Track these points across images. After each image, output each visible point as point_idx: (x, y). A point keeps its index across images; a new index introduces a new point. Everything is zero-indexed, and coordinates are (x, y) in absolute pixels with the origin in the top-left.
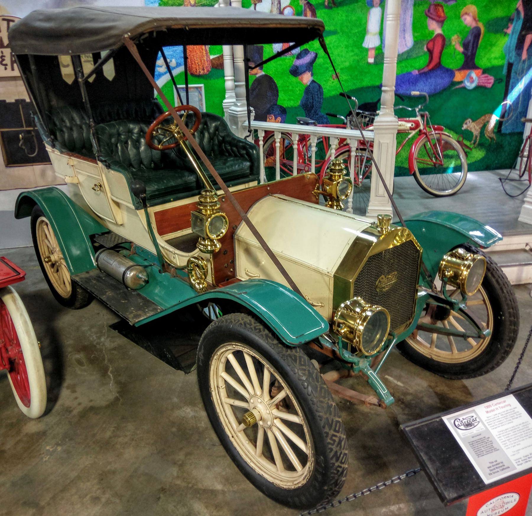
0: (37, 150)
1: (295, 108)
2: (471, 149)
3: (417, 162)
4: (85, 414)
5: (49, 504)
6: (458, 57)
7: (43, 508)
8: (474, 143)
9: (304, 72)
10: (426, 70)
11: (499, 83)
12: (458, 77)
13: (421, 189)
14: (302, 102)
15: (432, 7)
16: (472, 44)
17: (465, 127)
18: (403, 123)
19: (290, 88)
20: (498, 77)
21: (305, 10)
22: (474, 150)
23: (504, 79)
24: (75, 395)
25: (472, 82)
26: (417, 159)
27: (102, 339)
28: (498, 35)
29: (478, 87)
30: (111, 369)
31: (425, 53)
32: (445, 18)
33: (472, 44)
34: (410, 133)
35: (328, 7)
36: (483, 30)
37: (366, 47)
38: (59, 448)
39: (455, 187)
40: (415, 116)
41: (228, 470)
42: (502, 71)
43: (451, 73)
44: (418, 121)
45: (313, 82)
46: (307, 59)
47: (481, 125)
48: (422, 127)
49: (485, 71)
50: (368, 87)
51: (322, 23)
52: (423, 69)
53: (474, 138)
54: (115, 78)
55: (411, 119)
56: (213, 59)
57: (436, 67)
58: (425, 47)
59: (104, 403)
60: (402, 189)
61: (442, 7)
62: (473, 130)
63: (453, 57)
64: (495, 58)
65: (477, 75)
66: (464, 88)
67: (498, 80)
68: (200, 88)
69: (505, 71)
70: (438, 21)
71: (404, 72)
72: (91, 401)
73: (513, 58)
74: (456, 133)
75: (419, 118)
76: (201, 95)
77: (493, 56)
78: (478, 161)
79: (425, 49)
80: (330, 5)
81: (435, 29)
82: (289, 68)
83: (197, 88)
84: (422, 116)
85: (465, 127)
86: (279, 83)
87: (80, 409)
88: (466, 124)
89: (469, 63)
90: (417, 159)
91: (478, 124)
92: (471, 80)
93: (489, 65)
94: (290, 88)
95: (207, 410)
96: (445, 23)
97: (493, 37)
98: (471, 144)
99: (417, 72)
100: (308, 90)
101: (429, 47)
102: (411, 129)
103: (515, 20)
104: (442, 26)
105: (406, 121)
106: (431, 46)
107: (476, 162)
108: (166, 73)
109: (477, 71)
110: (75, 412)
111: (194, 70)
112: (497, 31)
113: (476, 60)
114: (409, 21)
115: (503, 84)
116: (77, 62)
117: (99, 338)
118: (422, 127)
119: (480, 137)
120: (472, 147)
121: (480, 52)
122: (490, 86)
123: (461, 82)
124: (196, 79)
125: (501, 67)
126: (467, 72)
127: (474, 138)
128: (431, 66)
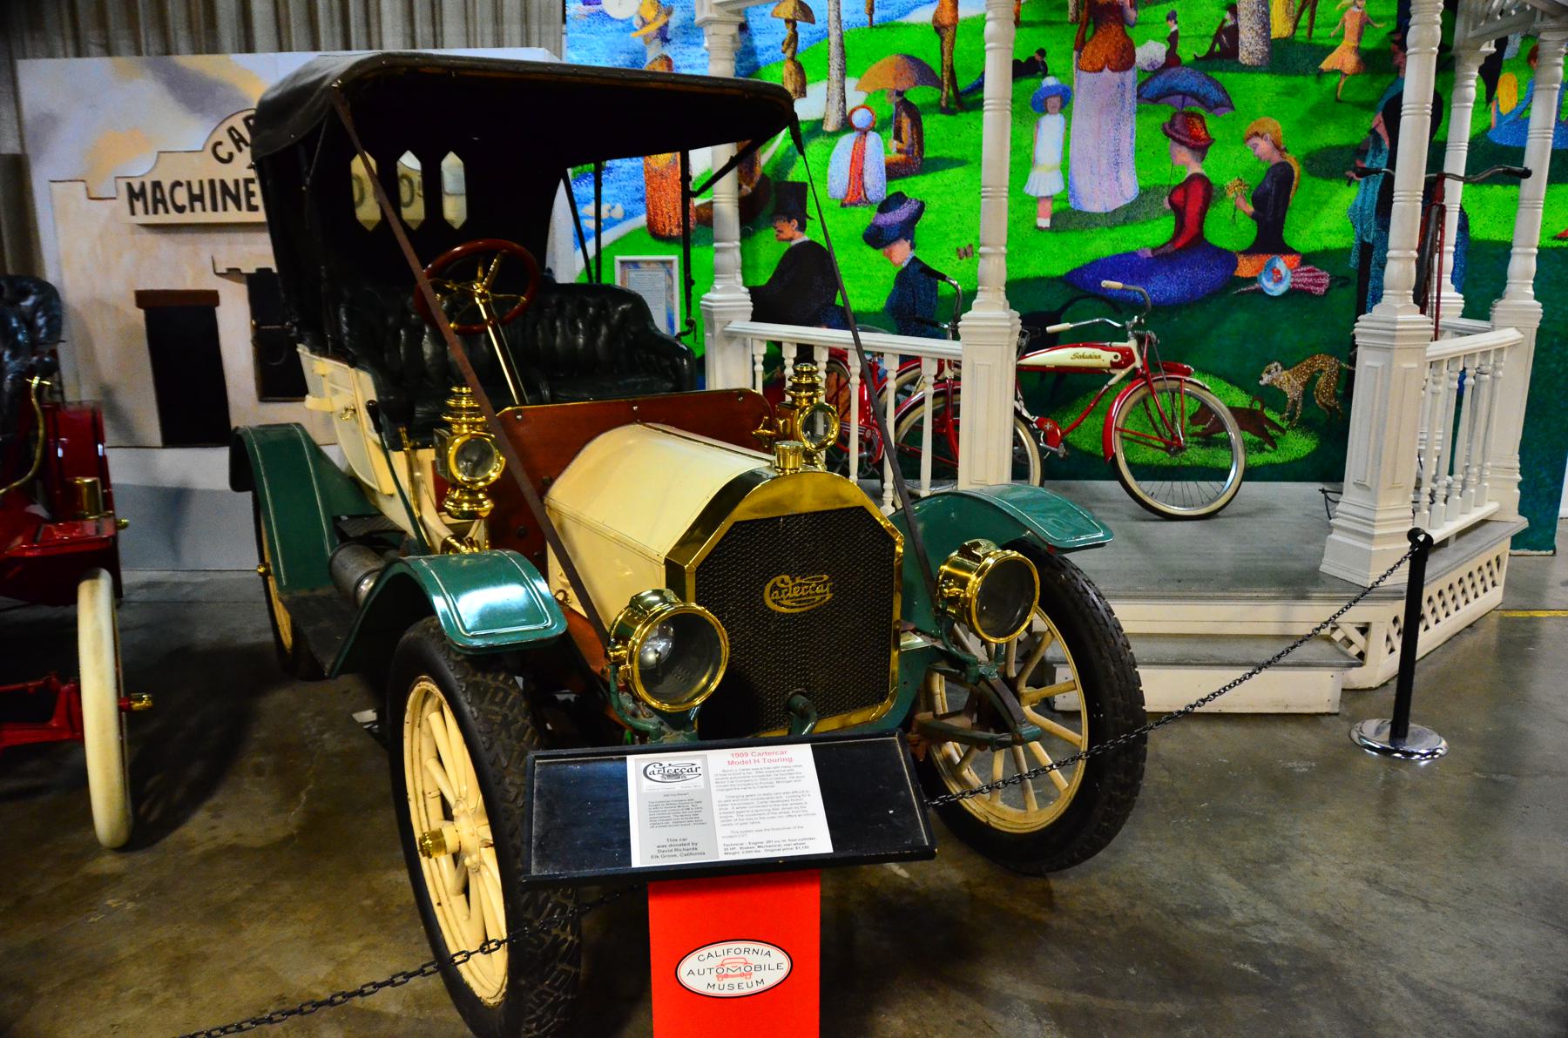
0: (723, 634)
1: (875, 313)
2: (1283, 431)
3: (1122, 437)
4: (209, 858)
5: (53, 993)
6: (1242, 225)
7: (40, 996)
8: (1291, 418)
9: (896, 239)
10: (1170, 249)
11: (1342, 286)
12: (1245, 268)
13: (1128, 497)
14: (890, 300)
15: (1179, 118)
16: (1272, 202)
17: (1266, 379)
18: (1097, 352)
19: (864, 270)
20: (1339, 273)
21: (897, 115)
22: (1289, 433)
23: (1354, 277)
24: (213, 822)
25: (1280, 280)
26: (1121, 430)
27: (326, 736)
28: (1333, 184)
29: (1292, 293)
30: (310, 786)
31: (1165, 214)
32: (1209, 141)
33: (1272, 202)
34: (1113, 376)
35: (946, 111)
36: (1297, 169)
37: (1033, 194)
38: (130, 906)
39: (1212, 501)
40: (1126, 339)
41: (247, 786)
42: (1348, 261)
43: (1227, 259)
44: (1130, 350)
45: (915, 260)
46: (900, 215)
47: (1305, 378)
48: (1138, 363)
49: (1307, 259)
50: (1039, 279)
51: (1377, 298)
52: (1163, 246)
53: (1289, 406)
54: (465, 225)
55: (1115, 344)
56: (701, 206)
57: (1190, 243)
58: (1166, 199)
59: (260, 843)
60: (1098, 500)
61: (1201, 118)
62: (1286, 388)
63: (1230, 227)
64: (1330, 232)
65: (1289, 266)
66: (1261, 292)
67: (1339, 281)
68: (671, 262)
69: (1354, 261)
70: (1193, 148)
71: (1120, 251)
72: (240, 835)
73: (1373, 234)
74: (1247, 392)
75: (1132, 344)
76: (671, 276)
77: (1323, 226)
78: (1303, 459)
79: (1167, 206)
80: (952, 106)
81: (1186, 166)
82: (862, 230)
83: (663, 262)
84: (1140, 340)
85: (1266, 379)
86: (841, 258)
87: (211, 845)
88: (1269, 372)
89: (1270, 240)
90: (1121, 430)
91: (1296, 376)
92: (1278, 278)
93: (1317, 246)
94: (864, 270)
95: (398, 813)
96: (1211, 150)
97: (1322, 186)
98: (1282, 420)
99: (1149, 254)
100: (903, 278)
101: (1175, 199)
102: (1115, 365)
103: (1371, 152)
104: (1203, 159)
105: (1104, 348)
106: (1179, 198)
107: (1296, 460)
108: (1393, 596)
109: (1289, 258)
110: (198, 851)
111: (660, 226)
112: (1330, 174)
113: (1286, 234)
114: (1126, 147)
115: (1352, 289)
116: (388, 180)
117: (322, 733)
118: (1138, 363)
119: (1305, 405)
120: (1284, 425)
121: (1293, 218)
122: (1321, 290)
123: (1254, 280)
124: (661, 245)
125: (1344, 253)
126: (1266, 259)
127: (1289, 406)
128: (1181, 242)
